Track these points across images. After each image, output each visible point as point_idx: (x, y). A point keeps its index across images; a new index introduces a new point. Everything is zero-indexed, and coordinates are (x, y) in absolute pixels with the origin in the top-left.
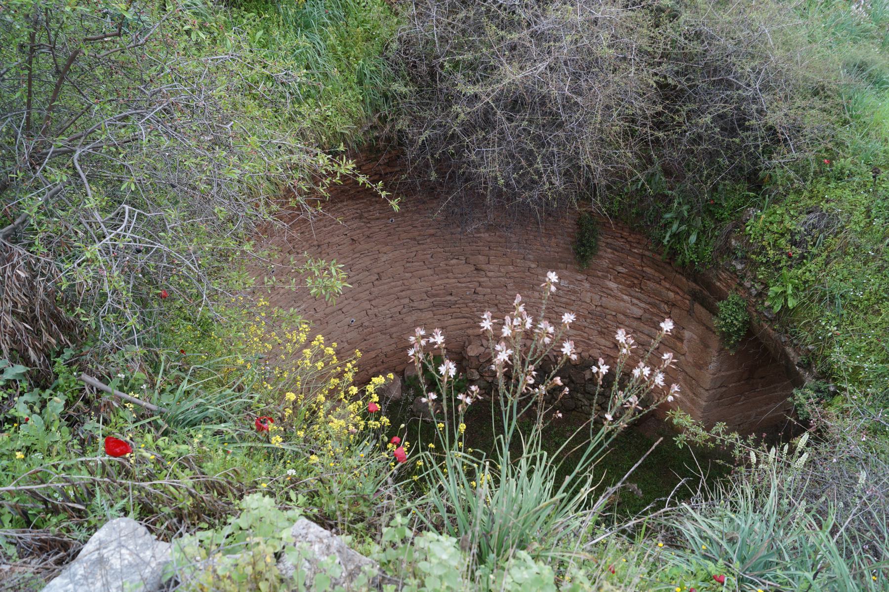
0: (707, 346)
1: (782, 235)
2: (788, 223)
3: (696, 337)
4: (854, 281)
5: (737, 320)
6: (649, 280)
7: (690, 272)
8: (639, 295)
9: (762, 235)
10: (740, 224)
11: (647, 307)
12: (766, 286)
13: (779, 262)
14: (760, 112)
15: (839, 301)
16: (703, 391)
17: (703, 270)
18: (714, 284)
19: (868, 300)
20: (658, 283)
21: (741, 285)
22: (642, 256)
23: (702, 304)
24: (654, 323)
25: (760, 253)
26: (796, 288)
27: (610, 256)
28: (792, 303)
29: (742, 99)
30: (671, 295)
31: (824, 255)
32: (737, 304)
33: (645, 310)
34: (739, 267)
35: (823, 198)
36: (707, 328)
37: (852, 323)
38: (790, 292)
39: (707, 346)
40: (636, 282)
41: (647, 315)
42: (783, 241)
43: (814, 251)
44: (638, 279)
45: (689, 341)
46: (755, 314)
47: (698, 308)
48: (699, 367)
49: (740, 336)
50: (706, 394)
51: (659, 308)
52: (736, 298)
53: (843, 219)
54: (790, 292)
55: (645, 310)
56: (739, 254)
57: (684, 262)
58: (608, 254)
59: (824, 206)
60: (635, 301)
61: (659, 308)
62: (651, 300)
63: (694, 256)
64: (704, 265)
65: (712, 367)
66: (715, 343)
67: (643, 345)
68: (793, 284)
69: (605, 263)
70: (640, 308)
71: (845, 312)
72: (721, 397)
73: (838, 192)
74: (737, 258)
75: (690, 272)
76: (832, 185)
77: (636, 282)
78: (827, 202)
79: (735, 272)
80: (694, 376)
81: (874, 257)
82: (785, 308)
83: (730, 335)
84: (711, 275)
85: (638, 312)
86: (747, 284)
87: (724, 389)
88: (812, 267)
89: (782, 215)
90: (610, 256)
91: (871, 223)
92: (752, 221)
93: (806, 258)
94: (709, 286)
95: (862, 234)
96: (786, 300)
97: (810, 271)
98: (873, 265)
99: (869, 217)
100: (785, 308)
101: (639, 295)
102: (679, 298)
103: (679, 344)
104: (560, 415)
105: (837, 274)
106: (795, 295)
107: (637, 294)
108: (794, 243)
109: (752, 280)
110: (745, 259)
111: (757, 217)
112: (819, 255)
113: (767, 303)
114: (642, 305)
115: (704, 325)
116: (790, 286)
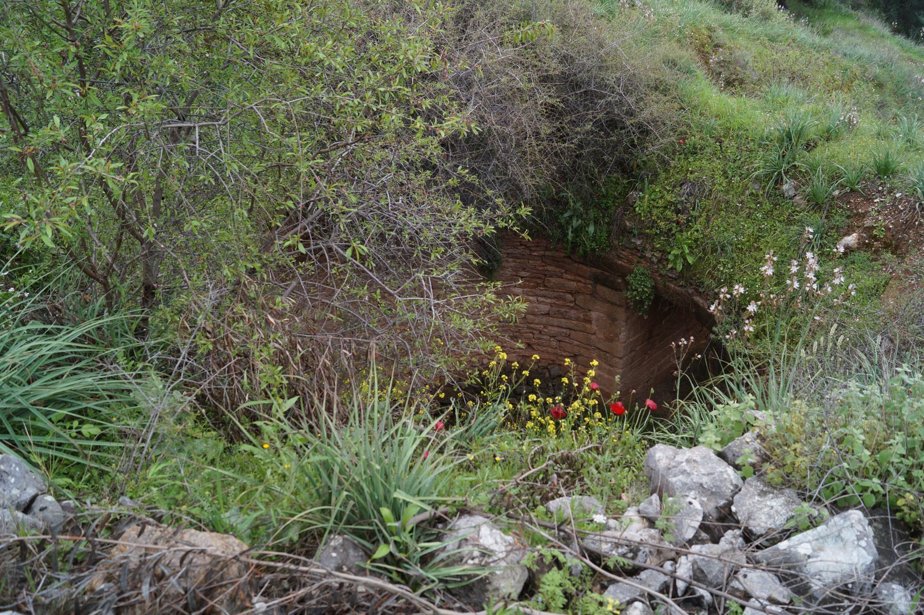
0: (614, 320)
1: (666, 207)
2: (668, 197)
3: (602, 315)
4: (734, 229)
5: (646, 287)
6: (551, 277)
7: (590, 259)
8: (544, 292)
9: (650, 212)
10: (629, 206)
11: (554, 301)
12: (664, 252)
13: (670, 230)
14: (630, 113)
15: (729, 248)
16: (617, 360)
17: (603, 254)
18: (616, 263)
19: (748, 241)
20: (560, 277)
21: (643, 257)
22: (542, 257)
23: (604, 285)
24: (562, 314)
25: (653, 227)
26: (690, 247)
27: (512, 264)
28: (690, 260)
29: (609, 104)
30: (574, 285)
31: (704, 214)
32: (643, 274)
33: (551, 305)
34: (639, 242)
35: (687, 170)
36: (612, 304)
37: (742, 263)
38: (687, 251)
39: (614, 320)
40: (539, 281)
41: (554, 309)
42: (668, 213)
43: (695, 213)
44: (540, 278)
45: (597, 320)
46: (659, 278)
47: (601, 289)
48: (611, 340)
49: (650, 299)
50: (621, 362)
51: (564, 300)
52: (642, 269)
53: (708, 184)
54: (687, 251)
55: (551, 305)
56: (636, 232)
57: (585, 252)
58: (511, 263)
59: (691, 177)
60: (541, 299)
61: (564, 300)
62: (556, 294)
63: (594, 244)
64: (603, 250)
65: (622, 336)
66: (621, 314)
67: (554, 337)
68: (688, 244)
69: (509, 272)
70: (546, 304)
71: (734, 255)
72: (633, 361)
73: (698, 163)
74: (634, 236)
75: (590, 259)
76: (691, 159)
77: (539, 281)
78: (691, 173)
79: (636, 248)
80: (607, 349)
81: (742, 208)
82: (687, 265)
83: (642, 302)
84: (611, 257)
85: (545, 308)
86: (648, 255)
87: (633, 353)
88: (698, 227)
89: (660, 192)
90: (512, 264)
91: (730, 182)
92: (638, 202)
93: (690, 221)
94: (610, 266)
95: (727, 192)
96: (685, 259)
97: (697, 231)
98: (744, 214)
99: (727, 177)
100: (687, 265)
101: (544, 292)
102: (582, 285)
103: (588, 326)
104: (699, 356)
105: (719, 227)
106: (691, 253)
107: (542, 293)
108: (678, 212)
109: (652, 251)
110: (641, 235)
111: (641, 199)
112: (700, 216)
113: (670, 266)
114: (549, 301)
115: (608, 302)
116: (686, 247)
